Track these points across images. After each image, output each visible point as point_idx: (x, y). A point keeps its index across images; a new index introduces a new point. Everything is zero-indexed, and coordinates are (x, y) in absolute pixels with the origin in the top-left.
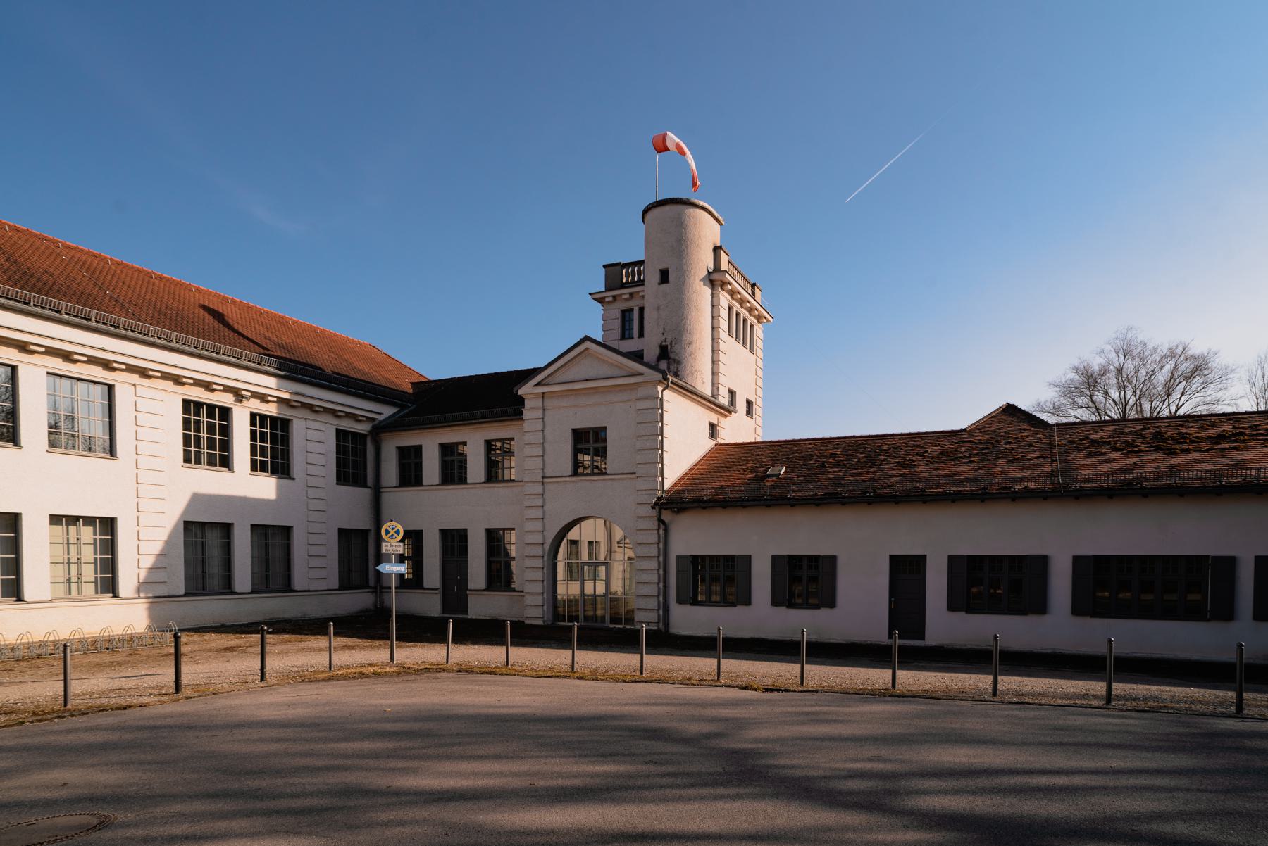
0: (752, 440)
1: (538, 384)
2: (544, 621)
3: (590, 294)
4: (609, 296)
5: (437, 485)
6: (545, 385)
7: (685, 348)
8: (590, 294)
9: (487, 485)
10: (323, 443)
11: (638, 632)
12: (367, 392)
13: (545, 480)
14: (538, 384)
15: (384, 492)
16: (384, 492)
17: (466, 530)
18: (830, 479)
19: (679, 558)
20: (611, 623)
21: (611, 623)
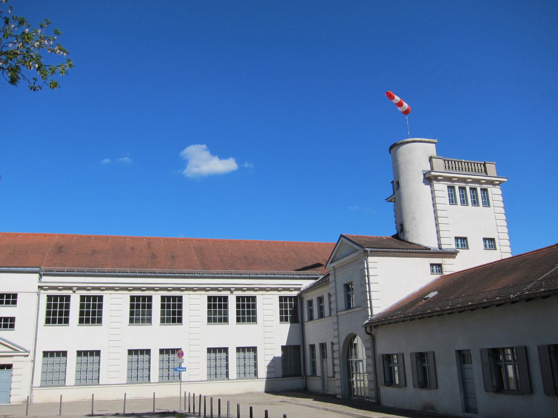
0: (500, 259)
1: (332, 262)
3: (385, 200)
8: (385, 200)
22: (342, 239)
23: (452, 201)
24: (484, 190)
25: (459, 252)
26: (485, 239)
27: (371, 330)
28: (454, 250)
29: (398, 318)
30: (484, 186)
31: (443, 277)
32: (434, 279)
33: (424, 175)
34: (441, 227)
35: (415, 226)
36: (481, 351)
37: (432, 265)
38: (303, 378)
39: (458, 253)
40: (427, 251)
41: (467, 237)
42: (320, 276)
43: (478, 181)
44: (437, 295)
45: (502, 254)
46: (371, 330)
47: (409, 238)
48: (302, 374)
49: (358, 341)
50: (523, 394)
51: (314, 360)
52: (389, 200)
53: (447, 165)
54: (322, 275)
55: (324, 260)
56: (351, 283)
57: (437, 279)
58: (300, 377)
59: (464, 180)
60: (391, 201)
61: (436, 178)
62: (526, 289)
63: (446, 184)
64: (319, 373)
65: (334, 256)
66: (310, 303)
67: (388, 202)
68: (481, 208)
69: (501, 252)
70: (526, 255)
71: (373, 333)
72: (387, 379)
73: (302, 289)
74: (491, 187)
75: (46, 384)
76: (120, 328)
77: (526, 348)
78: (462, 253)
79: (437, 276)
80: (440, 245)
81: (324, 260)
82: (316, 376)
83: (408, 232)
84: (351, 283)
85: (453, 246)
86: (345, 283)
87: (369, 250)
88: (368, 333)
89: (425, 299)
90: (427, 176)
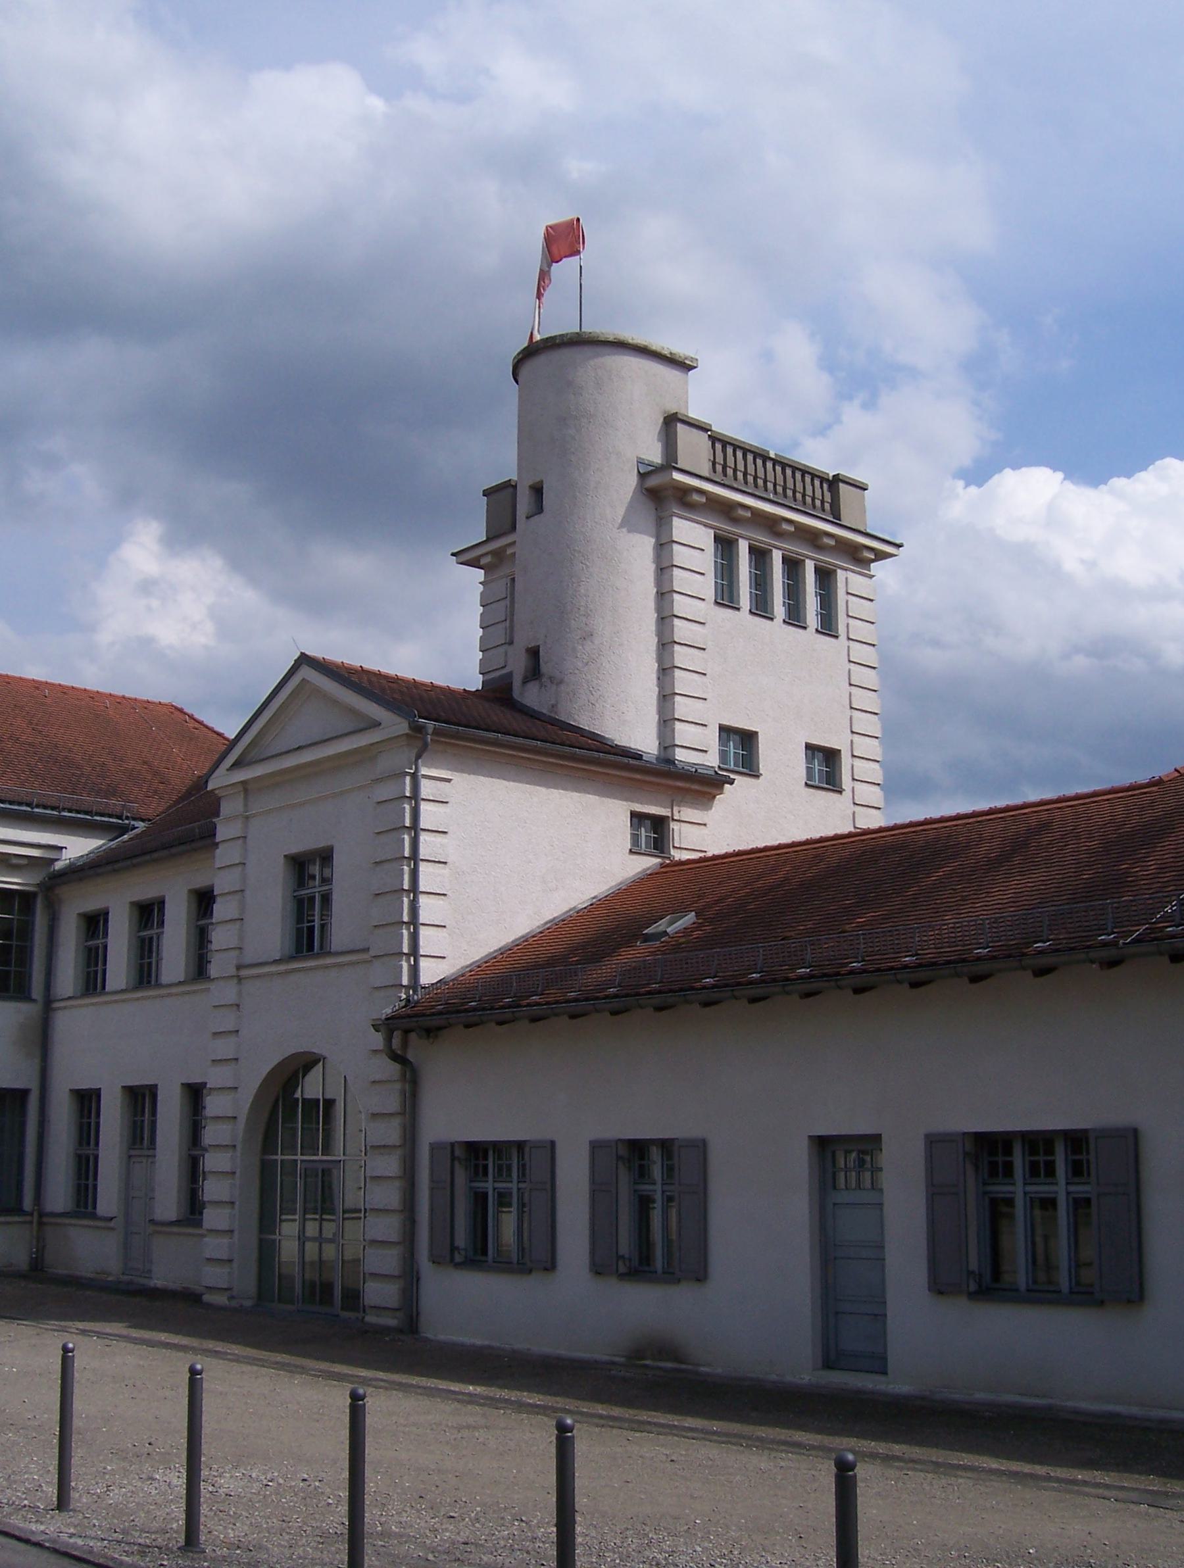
0: (847, 829)
1: (237, 765)
2: (232, 1298)
3: (453, 555)
4: (486, 554)
5: (123, 991)
6: (251, 763)
7: (574, 649)
8: (453, 555)
9: (139, 994)
10: (705, 825)
11: (1081, 1153)
12: (38, 806)
13: (244, 973)
14: (237, 765)
15: (59, 1008)
16: (59, 1008)
17: (156, 1086)
18: (413, 991)
19: (435, 1147)
20: (342, 1309)
21: (342, 1309)
22: (306, 672)
23: (726, 597)
24: (825, 577)
25: (732, 782)
26: (809, 747)
27: (405, 1044)
28: (713, 773)
29: (548, 1003)
30: (829, 559)
31: (668, 866)
32: (639, 870)
33: (642, 476)
34: (682, 682)
35: (587, 664)
36: (934, 1142)
37: (634, 815)
38: (31, 1222)
39: (727, 786)
40: (632, 761)
41: (756, 733)
42: (136, 824)
43: (812, 538)
44: (696, 926)
45: (858, 809)
46: (405, 1044)
47: (559, 706)
48: (28, 1203)
49: (94, 1097)
50: (1101, 1303)
51: (90, 1152)
52: (467, 557)
53: (720, 459)
54: (143, 820)
55: (145, 763)
56: (326, 856)
57: (648, 872)
58: (16, 1219)
59: (771, 524)
60: (474, 563)
61: (684, 498)
62: (1159, 916)
63: (711, 527)
64: (108, 1199)
65: (253, 743)
66: (95, 923)
67: (461, 563)
68: (808, 638)
69: (855, 804)
70: (979, 819)
71: (410, 1056)
72: (626, 1243)
73: (58, 865)
74: (846, 569)
75: (140, 1233)
76: (703, 574)
77: (1135, 1132)
78: (739, 790)
79: (649, 863)
80: (667, 744)
81: (145, 763)
82: (93, 1216)
83: (561, 682)
84: (326, 856)
85: (712, 760)
86: (295, 849)
87: (430, 725)
88: (395, 1057)
89: (647, 938)
90: (653, 482)
